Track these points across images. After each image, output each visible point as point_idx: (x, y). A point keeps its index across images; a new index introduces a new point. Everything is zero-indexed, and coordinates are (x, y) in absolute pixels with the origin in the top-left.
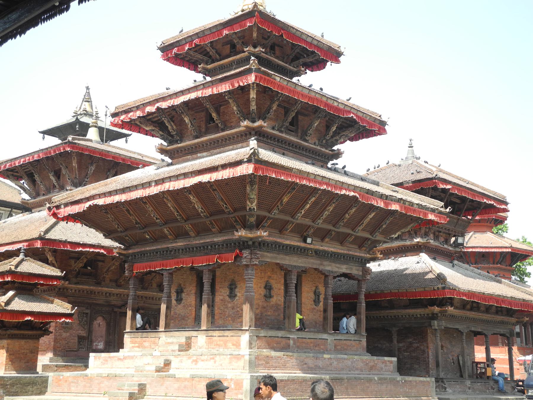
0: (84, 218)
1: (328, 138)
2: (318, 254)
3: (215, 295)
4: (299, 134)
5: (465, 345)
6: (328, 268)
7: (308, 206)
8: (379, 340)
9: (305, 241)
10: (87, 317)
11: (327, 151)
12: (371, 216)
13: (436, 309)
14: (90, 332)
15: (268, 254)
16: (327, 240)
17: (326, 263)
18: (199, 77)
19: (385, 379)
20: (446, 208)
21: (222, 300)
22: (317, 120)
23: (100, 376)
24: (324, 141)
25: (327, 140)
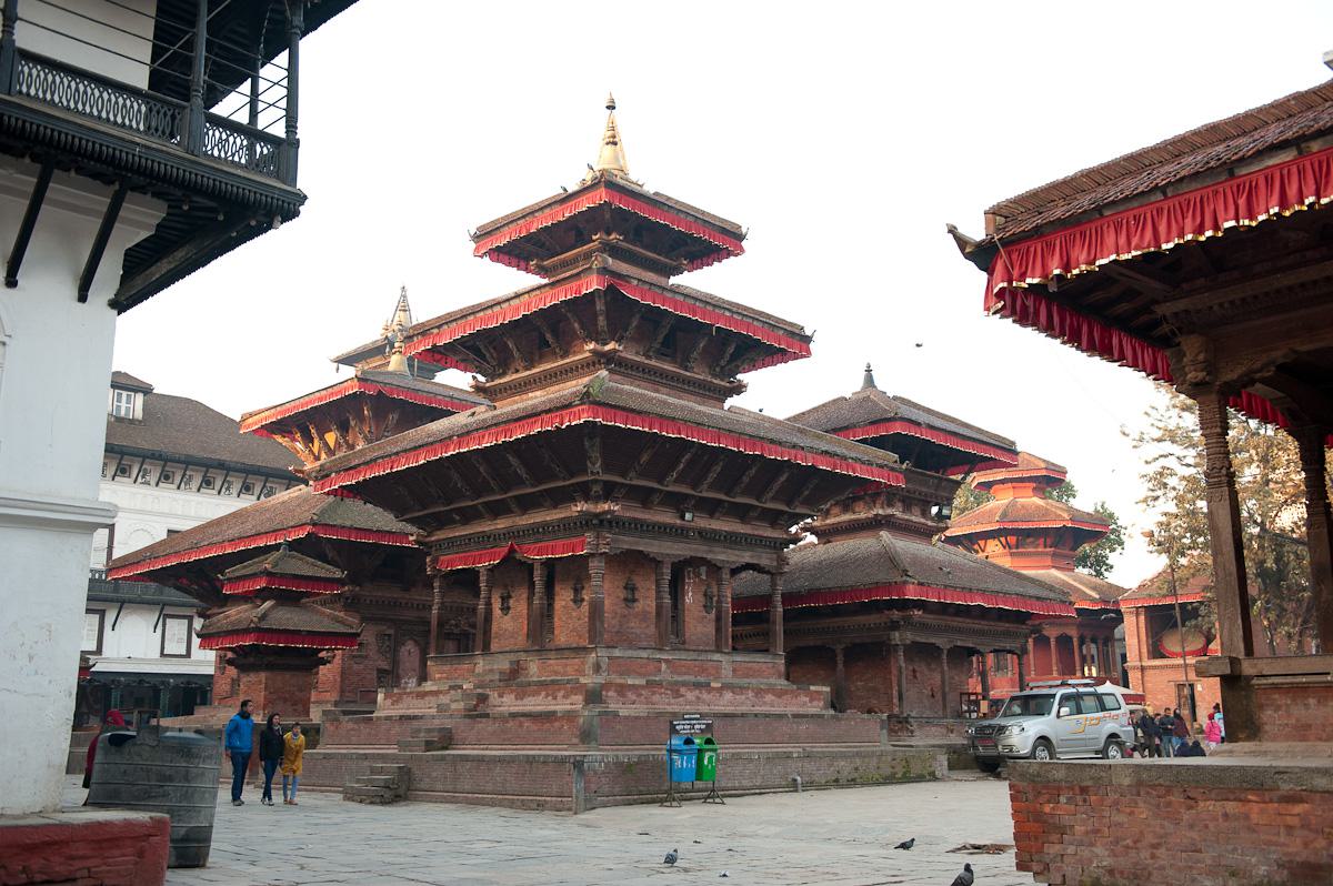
0: (366, 492)
1: (723, 363)
2: (706, 536)
3: (553, 599)
4: (679, 360)
5: (946, 668)
6: (722, 557)
7: (682, 466)
8: (804, 661)
9: (683, 518)
10: (389, 640)
11: (723, 383)
12: (783, 478)
13: (896, 614)
14: (395, 662)
15: (626, 539)
16: (717, 515)
17: (716, 549)
18: (535, 280)
19: (659, 684)
20: (902, 463)
21: (564, 607)
22: (703, 338)
23: (388, 718)
24: (718, 369)
25: (722, 368)
